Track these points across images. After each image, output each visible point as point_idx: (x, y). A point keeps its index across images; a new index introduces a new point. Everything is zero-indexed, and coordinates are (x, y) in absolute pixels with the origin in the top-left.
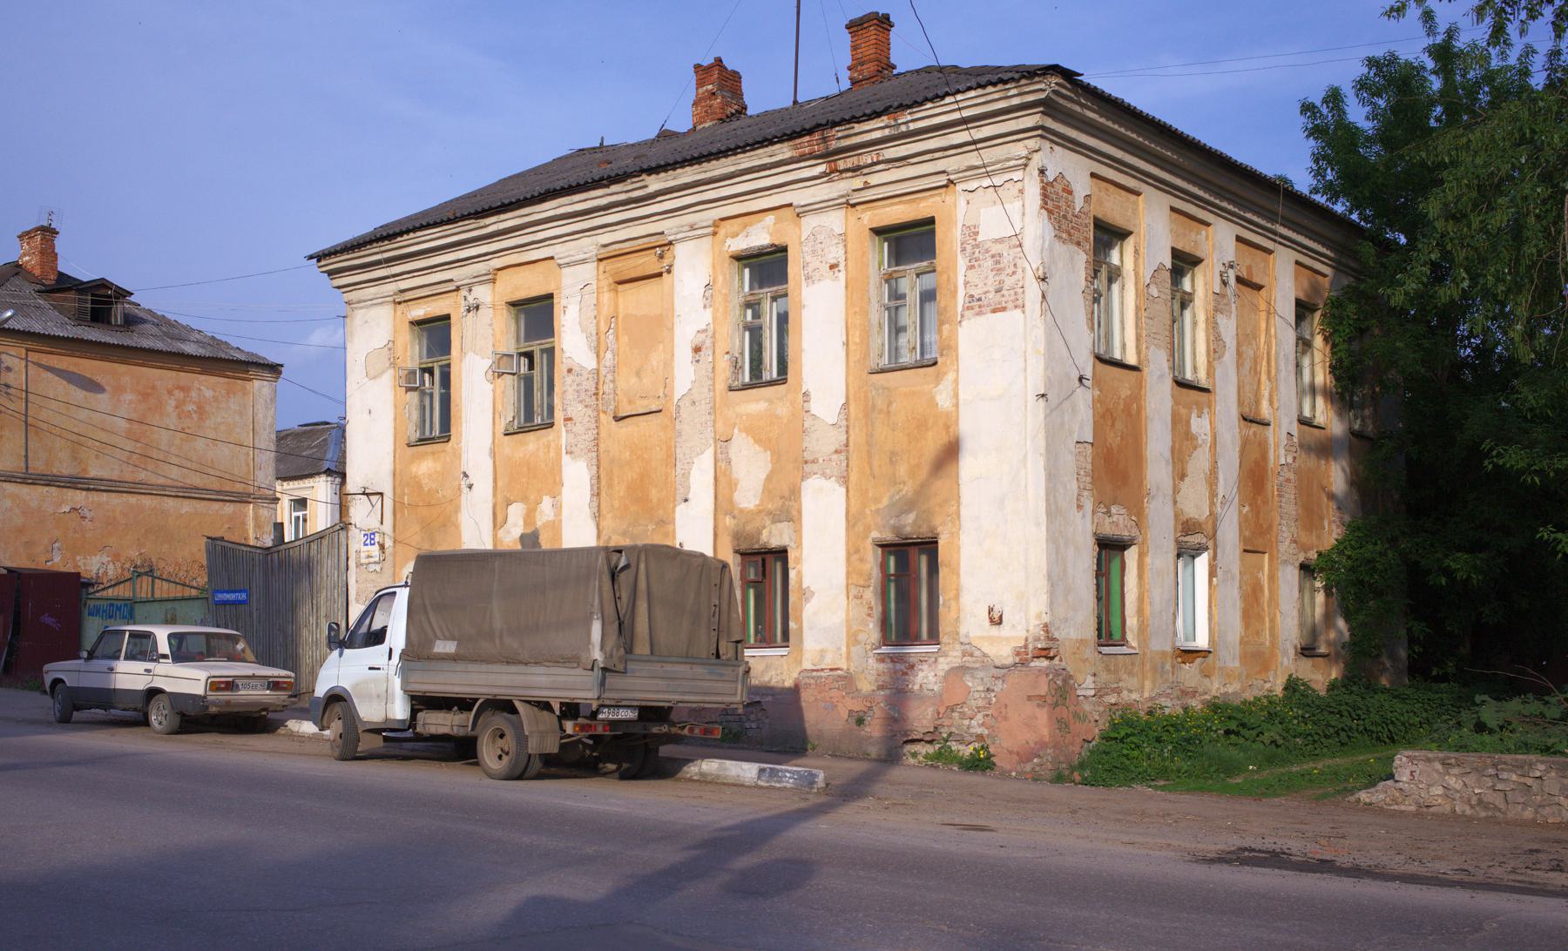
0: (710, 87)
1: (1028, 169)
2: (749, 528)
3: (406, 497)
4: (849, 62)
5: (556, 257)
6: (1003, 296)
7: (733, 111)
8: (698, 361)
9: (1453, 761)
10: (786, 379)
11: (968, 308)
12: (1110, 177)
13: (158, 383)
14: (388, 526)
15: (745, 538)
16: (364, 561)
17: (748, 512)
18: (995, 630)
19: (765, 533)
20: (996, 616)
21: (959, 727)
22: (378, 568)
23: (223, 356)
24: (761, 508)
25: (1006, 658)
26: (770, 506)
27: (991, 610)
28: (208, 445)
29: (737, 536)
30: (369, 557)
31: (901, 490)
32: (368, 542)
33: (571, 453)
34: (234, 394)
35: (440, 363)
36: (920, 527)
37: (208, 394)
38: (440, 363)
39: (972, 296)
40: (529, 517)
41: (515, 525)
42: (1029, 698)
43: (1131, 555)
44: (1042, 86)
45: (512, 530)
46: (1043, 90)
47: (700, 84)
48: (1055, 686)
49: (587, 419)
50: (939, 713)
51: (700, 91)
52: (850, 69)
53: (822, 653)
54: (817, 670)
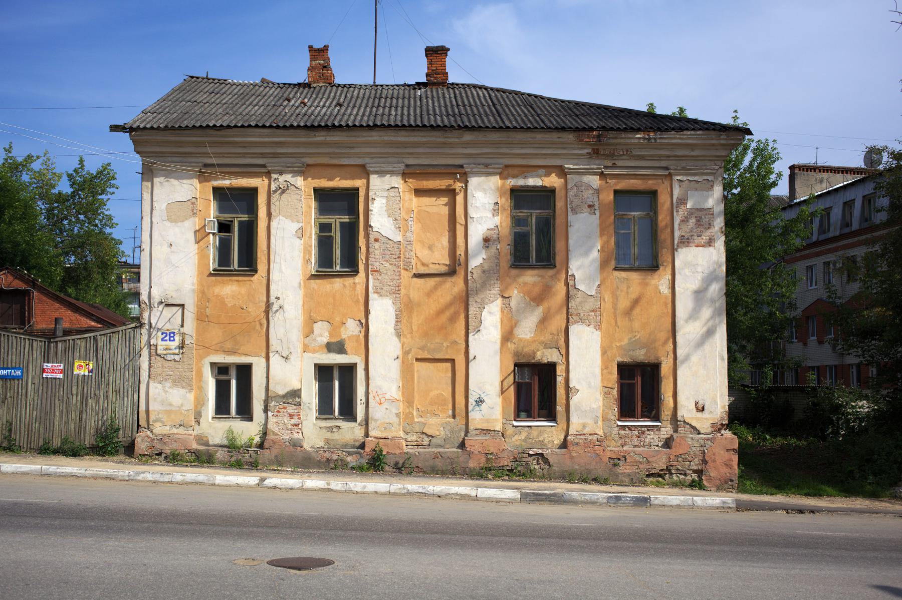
0: (322, 62)
6: (702, 239)
8: (487, 247)
11: (681, 242)
12: (647, 165)
15: (524, 356)
17: (525, 341)
18: (699, 415)
20: (700, 407)
22: (177, 358)
25: (707, 429)
26: (542, 338)
27: (696, 404)
31: (636, 336)
35: (239, 219)
36: (649, 357)
38: (239, 219)
40: (334, 330)
42: (728, 450)
45: (318, 339)
50: (670, 458)
54: (580, 435)
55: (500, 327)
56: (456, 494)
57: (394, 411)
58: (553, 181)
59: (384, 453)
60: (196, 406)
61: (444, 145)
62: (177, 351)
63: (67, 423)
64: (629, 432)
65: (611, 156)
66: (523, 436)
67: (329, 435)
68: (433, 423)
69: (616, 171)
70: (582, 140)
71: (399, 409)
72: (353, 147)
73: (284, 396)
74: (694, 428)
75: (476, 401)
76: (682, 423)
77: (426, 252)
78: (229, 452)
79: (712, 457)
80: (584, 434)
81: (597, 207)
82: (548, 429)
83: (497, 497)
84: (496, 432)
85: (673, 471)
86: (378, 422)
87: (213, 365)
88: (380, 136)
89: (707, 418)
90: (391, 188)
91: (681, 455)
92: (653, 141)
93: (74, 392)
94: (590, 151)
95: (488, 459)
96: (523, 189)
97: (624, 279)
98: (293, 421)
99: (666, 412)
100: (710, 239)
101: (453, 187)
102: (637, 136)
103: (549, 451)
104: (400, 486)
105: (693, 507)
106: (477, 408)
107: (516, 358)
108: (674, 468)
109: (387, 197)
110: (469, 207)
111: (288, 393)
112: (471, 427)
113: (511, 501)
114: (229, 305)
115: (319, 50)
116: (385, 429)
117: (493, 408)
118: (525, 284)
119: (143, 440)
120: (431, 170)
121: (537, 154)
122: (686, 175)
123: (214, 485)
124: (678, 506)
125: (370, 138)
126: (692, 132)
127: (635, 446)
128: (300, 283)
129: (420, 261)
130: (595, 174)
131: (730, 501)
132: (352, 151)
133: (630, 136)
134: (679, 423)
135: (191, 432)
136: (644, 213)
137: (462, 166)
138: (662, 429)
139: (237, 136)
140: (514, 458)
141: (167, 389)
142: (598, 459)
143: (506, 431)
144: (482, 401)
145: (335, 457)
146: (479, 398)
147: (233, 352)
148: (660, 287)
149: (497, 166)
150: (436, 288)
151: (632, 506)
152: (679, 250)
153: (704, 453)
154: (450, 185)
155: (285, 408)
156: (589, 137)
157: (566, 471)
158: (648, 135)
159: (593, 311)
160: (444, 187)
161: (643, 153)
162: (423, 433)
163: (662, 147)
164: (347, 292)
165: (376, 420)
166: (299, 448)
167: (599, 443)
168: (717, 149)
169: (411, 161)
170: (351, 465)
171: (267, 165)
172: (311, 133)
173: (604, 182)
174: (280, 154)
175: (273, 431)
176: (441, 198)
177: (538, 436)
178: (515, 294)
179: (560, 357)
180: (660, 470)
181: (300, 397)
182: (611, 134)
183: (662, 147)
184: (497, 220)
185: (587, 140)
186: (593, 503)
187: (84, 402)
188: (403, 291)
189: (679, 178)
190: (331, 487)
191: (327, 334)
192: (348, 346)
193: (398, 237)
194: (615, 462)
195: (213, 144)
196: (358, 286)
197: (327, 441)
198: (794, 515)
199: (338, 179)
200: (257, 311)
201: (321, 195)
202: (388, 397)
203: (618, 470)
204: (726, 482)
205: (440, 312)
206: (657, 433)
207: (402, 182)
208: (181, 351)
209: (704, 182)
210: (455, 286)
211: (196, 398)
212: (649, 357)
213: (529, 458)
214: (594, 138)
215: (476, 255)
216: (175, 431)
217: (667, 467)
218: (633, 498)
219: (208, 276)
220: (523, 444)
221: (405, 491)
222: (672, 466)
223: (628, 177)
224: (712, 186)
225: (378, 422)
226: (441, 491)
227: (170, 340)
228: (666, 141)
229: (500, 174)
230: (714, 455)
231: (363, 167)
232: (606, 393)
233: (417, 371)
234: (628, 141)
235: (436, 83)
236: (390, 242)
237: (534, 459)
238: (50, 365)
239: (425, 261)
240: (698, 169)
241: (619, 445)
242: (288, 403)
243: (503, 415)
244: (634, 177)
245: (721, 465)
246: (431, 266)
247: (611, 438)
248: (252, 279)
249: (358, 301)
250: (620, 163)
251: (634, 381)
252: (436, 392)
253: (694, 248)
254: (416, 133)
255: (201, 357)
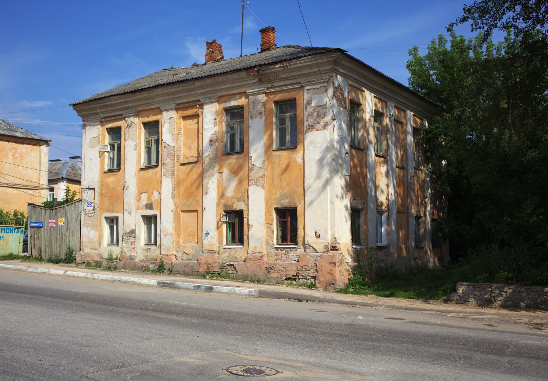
0: (212, 50)
1: (329, 82)
2: (229, 203)
3: (103, 190)
4: (261, 43)
5: (161, 107)
6: (320, 125)
7: (220, 58)
9: (477, 286)
10: (243, 151)
11: (308, 129)
13: (6, 147)
14: (96, 201)
16: (87, 212)
18: (317, 240)
19: (235, 205)
21: (305, 273)
22: (92, 215)
23: (30, 137)
24: (234, 196)
26: (237, 196)
27: (316, 233)
28: (23, 169)
29: (225, 206)
30: (89, 211)
31: (284, 191)
32: (89, 206)
33: (165, 176)
34: (33, 151)
37: (24, 151)
39: (309, 125)
40: (149, 198)
41: (144, 201)
43: (363, 214)
44: (335, 55)
45: (143, 202)
46: (335, 57)
47: (208, 49)
48: (339, 260)
49: (171, 164)
50: (298, 268)
51: (208, 51)
52: (261, 45)
53: (256, 247)
54: (254, 253)
55: (216, 190)
56: (132, 281)
57: (171, 240)
58: (242, 101)
59: (164, 263)
60: (99, 239)
61: (190, 90)
62: (92, 212)
63: (57, 248)
64: (280, 251)
65: (269, 81)
66: (227, 254)
67: (146, 253)
68: (188, 246)
69: (273, 90)
70: (250, 75)
71: (173, 239)
72: (154, 99)
73: (129, 233)
74: (314, 249)
75: (205, 234)
76: (308, 245)
77: (188, 151)
78: (108, 262)
79: (321, 268)
80: (256, 253)
81: (263, 114)
82: (239, 250)
83: (147, 283)
84: (215, 252)
85: (300, 277)
86: (165, 246)
87: (106, 218)
88: (161, 91)
89: (321, 243)
90: (171, 118)
91: (304, 266)
92: (286, 68)
93: (59, 233)
94: (257, 80)
95: (208, 267)
96: (229, 108)
97: (278, 156)
98: (133, 246)
99: (300, 239)
100: (325, 125)
101: (198, 113)
102: (277, 66)
103: (237, 263)
104: (112, 276)
105: (233, 294)
106: (206, 238)
107: (224, 208)
108: (300, 274)
109: (169, 123)
110: (204, 123)
111: (130, 231)
112: (204, 249)
113: (152, 286)
114: (111, 187)
115: (211, 43)
116: (168, 250)
117: (213, 238)
118: (230, 164)
119: (79, 256)
120: (187, 105)
121: (233, 87)
122: (312, 85)
123: (49, 274)
124: (227, 293)
125: (157, 93)
126: (306, 58)
127: (284, 260)
128: (135, 174)
129: (185, 156)
130: (262, 93)
131: (253, 291)
132: (153, 101)
133: (273, 67)
134: (306, 246)
135: (97, 252)
136: (293, 113)
137: (199, 101)
138: (298, 250)
139: (107, 102)
140: (220, 267)
141: (89, 231)
142: (260, 268)
143: (220, 251)
144: (208, 234)
145: (145, 265)
146: (207, 232)
147: (112, 211)
148: (297, 159)
149: (214, 98)
150: (191, 170)
151: (205, 292)
152: (306, 134)
153: (316, 265)
154: (197, 112)
155: (129, 239)
156: (253, 72)
157: (244, 275)
158: (283, 64)
159: (261, 177)
160: (194, 114)
161: (285, 76)
162: (184, 252)
163: (293, 70)
164: (154, 176)
165: (164, 245)
166: (132, 260)
167: (261, 258)
168: (326, 65)
169: (179, 102)
170: (152, 269)
171: (123, 114)
172: (134, 95)
173: (267, 97)
174: (128, 107)
175: (124, 252)
176: (195, 120)
177: (234, 254)
178: (226, 172)
179: (245, 206)
180: (293, 276)
181: (135, 233)
182: (264, 68)
183: (293, 70)
184: (216, 129)
185: (253, 74)
186: (187, 289)
187: (62, 238)
188: (176, 174)
189: (308, 88)
190: (87, 276)
191: (146, 200)
192: (154, 206)
193: (173, 144)
194: (269, 269)
195: (100, 108)
196: (158, 173)
197: (146, 256)
198: (259, 299)
199: (151, 116)
200: (119, 189)
201: (145, 124)
202: (169, 232)
203: (270, 275)
204: (330, 285)
205: (192, 184)
206: (295, 252)
207: (176, 113)
208: (94, 212)
209: (322, 88)
210: (197, 170)
211: (99, 235)
212: (291, 203)
213: (228, 267)
214: (256, 72)
215: (206, 151)
216: (91, 251)
217: (297, 274)
218: (206, 287)
219: (104, 173)
220: (227, 258)
221: (113, 279)
222: (299, 273)
223: (280, 92)
224: (326, 90)
225: (165, 246)
226: (126, 280)
227: (90, 207)
228: (293, 66)
229: (218, 101)
230: (322, 266)
231: (159, 108)
232: (268, 227)
233: (183, 217)
234: (273, 70)
235: (265, 49)
236: (170, 147)
237: (230, 268)
238: (51, 220)
239: (187, 156)
240: (317, 80)
241: (275, 260)
242: (130, 237)
243: (218, 242)
244: (283, 92)
245: (327, 273)
246: (190, 158)
247: (270, 256)
248: (119, 173)
249: (158, 181)
250: (275, 85)
251: (286, 220)
252: (191, 229)
253: (315, 132)
254: (175, 86)
255: (101, 215)
